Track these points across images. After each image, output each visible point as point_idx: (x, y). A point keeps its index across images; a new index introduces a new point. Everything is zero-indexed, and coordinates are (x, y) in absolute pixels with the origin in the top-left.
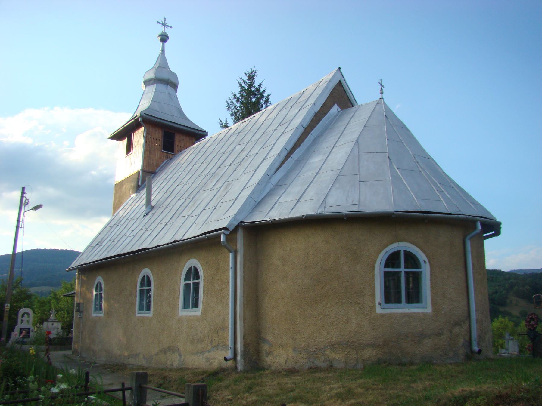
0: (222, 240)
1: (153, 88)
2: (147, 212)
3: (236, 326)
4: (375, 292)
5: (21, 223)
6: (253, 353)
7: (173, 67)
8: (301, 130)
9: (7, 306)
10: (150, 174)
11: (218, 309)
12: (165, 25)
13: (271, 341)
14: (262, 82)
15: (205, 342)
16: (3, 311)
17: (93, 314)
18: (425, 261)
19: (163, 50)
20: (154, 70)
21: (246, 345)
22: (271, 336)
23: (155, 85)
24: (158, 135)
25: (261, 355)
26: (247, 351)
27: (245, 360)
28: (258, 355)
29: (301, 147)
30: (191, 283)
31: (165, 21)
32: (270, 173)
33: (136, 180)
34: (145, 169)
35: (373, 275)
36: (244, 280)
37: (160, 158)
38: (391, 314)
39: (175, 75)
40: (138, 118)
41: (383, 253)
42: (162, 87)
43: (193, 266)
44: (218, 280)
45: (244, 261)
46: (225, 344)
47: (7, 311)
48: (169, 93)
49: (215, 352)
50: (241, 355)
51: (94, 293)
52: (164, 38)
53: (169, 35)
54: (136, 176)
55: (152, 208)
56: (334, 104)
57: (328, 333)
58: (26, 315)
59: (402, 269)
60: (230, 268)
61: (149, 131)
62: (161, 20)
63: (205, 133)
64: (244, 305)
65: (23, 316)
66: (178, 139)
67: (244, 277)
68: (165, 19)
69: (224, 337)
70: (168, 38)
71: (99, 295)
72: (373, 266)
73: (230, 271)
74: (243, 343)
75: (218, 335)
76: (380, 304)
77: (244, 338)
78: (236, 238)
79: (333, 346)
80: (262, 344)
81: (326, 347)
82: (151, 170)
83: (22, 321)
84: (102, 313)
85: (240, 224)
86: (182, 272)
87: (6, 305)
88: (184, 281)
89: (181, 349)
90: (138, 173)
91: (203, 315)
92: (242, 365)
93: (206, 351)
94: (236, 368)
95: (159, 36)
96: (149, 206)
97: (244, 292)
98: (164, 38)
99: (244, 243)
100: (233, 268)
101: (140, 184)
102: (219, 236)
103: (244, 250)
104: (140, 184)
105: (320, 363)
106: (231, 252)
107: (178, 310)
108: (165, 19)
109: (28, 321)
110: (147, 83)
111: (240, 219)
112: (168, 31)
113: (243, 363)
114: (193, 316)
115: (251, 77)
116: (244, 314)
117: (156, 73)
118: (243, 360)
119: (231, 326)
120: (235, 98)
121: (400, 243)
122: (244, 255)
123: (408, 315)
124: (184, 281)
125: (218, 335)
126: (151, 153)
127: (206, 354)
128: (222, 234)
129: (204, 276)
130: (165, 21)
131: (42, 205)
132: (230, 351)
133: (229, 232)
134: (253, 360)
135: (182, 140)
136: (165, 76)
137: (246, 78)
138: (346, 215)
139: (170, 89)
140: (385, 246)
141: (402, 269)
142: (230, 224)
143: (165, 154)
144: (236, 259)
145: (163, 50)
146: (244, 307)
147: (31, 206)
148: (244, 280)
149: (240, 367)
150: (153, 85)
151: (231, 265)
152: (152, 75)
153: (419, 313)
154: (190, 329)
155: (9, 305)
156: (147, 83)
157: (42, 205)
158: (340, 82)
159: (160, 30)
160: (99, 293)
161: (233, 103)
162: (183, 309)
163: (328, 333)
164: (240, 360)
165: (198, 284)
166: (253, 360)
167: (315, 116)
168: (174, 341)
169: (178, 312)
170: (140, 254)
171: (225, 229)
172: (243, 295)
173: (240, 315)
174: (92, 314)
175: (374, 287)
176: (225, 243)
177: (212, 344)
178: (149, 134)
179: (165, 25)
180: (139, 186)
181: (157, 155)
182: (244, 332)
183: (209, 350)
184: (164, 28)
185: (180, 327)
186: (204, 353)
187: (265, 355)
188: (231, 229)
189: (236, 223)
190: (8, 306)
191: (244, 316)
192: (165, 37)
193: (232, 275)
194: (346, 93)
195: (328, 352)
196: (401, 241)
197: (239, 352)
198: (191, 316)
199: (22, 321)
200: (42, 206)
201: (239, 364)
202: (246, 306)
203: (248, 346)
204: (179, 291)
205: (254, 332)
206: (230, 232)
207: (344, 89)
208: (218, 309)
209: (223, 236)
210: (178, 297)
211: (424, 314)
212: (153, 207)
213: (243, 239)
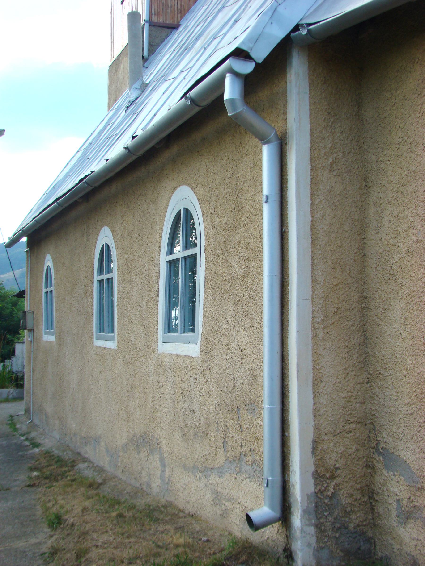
0: (227, 96)
2: (132, 98)
3: (289, 403)
6: (349, 500)
10: (167, 30)
11: (238, 341)
13: (417, 467)
15: (210, 440)
17: (44, 335)
22: (417, 451)
25: (381, 511)
26: (329, 493)
27: (318, 526)
28: (372, 509)
30: (179, 258)
36: (313, 241)
43: (184, 208)
44: (239, 243)
45: (313, 169)
46: (258, 458)
49: (233, 480)
50: (305, 511)
60: (264, 199)
64: (314, 329)
67: (313, 226)
69: (257, 435)
71: (49, 293)
73: (266, 208)
74: (312, 469)
75: (240, 427)
77: (314, 449)
78: (285, 93)
80: (385, 472)
82: (169, 21)
84: (112, 339)
85: (292, 35)
86: (162, 229)
88: (167, 255)
89: (164, 447)
91: (204, 357)
92: (309, 545)
93: (212, 469)
96: (137, 85)
97: (314, 281)
99: (313, 104)
100: (275, 199)
103: (311, 130)
106: (264, 140)
107: (155, 336)
113: (313, 540)
114: (185, 357)
118: (312, 530)
119: (271, 403)
122: (312, 149)
124: (167, 255)
125: (240, 427)
127: (214, 479)
128: (228, 75)
129: (207, 236)
131: (4, 130)
133: (254, 64)
134: (351, 526)
144: (286, 165)
146: (315, 336)
151: (266, 190)
154: (178, 394)
157: (4, 130)
162: (165, 333)
164: (302, 530)
165: (194, 257)
166: (351, 526)
168: (152, 419)
169: (157, 342)
172: (309, 294)
173: (298, 365)
174: (42, 335)
176: (241, 108)
177: (226, 451)
182: (317, 428)
183: (219, 468)
185: (161, 384)
186: (209, 473)
187: (394, 513)
191: (314, 368)
193: (271, 224)
197: (299, 499)
198: (179, 356)
200: (5, 133)
201: (299, 542)
202: (321, 335)
203: (332, 477)
204: (158, 282)
205: (353, 426)
206: (257, 65)
208: (238, 341)
209: (232, 84)
210: (156, 299)
212: (146, 87)
213: (308, 91)
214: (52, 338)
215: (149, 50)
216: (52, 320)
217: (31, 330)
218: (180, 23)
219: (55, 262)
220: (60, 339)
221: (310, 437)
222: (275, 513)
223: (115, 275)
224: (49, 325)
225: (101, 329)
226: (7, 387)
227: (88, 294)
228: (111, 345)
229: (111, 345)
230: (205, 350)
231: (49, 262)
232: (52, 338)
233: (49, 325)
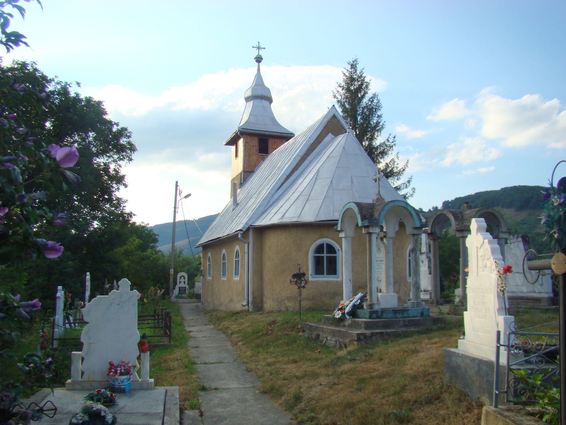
0: (239, 237)
1: (251, 104)
2: (234, 208)
4: (308, 268)
5: (177, 209)
7: (267, 84)
8: (299, 158)
9: (172, 271)
12: (259, 48)
14: (363, 69)
16: (169, 274)
18: (338, 250)
19: (259, 70)
20: (251, 89)
21: (254, 298)
23: (252, 101)
24: (255, 142)
29: (298, 170)
31: (259, 44)
32: (272, 193)
33: (239, 179)
34: (246, 170)
35: (308, 258)
37: (257, 160)
38: (317, 281)
39: (268, 90)
40: (237, 132)
41: (315, 244)
42: (258, 102)
47: (172, 275)
48: (264, 106)
50: (251, 303)
51: (208, 263)
52: (259, 59)
53: (263, 57)
54: (239, 176)
55: (237, 204)
56: (329, 133)
57: (286, 291)
58: (182, 278)
59: (325, 255)
61: (247, 140)
62: (256, 44)
63: (292, 135)
64: (253, 275)
65: (181, 278)
66: (271, 142)
68: (259, 42)
70: (262, 59)
72: (308, 253)
76: (311, 275)
79: (288, 299)
81: (285, 299)
83: (180, 282)
84: (225, 278)
87: (171, 270)
90: (241, 173)
94: (248, 310)
95: (255, 59)
96: (235, 204)
98: (259, 59)
101: (242, 182)
102: (237, 235)
104: (242, 182)
105: (283, 309)
106: (246, 243)
108: (259, 42)
109: (184, 282)
110: (247, 99)
111: (250, 223)
112: (262, 53)
115: (353, 66)
116: (253, 279)
117: (252, 92)
118: (252, 306)
120: (340, 87)
121: (323, 239)
123: (327, 282)
126: (250, 157)
130: (259, 44)
132: (245, 301)
135: (275, 143)
136: (259, 93)
137: (349, 67)
138: (291, 224)
139: (265, 103)
140: (315, 241)
141: (325, 255)
142: (244, 227)
143: (261, 156)
145: (259, 70)
147: (183, 195)
148: (253, 260)
149: (251, 310)
150: (250, 102)
152: (249, 94)
153: (334, 281)
155: (173, 270)
156: (247, 99)
158: (334, 115)
159: (255, 53)
160: (237, 259)
161: (338, 92)
163: (286, 291)
167: (310, 146)
170: (220, 240)
171: (240, 230)
175: (308, 265)
178: (247, 143)
179: (259, 48)
180: (241, 183)
181: (255, 158)
184: (259, 50)
188: (244, 230)
189: (247, 226)
190: (172, 271)
192: (259, 59)
194: (339, 122)
195: (286, 302)
196: (324, 237)
199: (180, 282)
203: (256, 298)
207: (338, 120)
211: (337, 281)
214: (210, 278)
215: (243, 180)
216: (267, 209)
217: (204, 276)
218: (255, 170)
219: (211, 255)
220: (213, 278)
221: (252, 291)
222: (247, 304)
223: (226, 261)
224: (237, 273)
225: (223, 275)
226: (193, 299)
227: (220, 266)
228: (225, 279)
229: (225, 279)
230: (240, 279)
231: (209, 254)
232: (210, 278)
233: (210, 274)
